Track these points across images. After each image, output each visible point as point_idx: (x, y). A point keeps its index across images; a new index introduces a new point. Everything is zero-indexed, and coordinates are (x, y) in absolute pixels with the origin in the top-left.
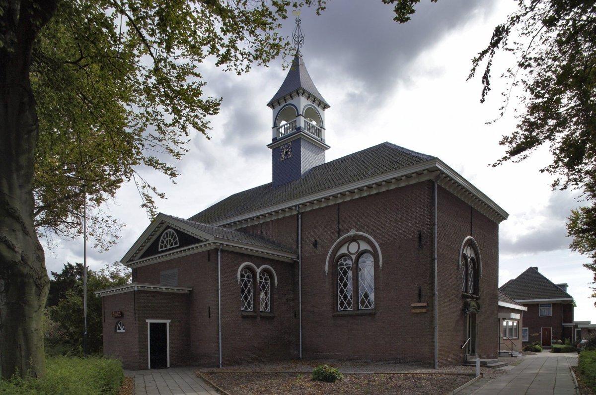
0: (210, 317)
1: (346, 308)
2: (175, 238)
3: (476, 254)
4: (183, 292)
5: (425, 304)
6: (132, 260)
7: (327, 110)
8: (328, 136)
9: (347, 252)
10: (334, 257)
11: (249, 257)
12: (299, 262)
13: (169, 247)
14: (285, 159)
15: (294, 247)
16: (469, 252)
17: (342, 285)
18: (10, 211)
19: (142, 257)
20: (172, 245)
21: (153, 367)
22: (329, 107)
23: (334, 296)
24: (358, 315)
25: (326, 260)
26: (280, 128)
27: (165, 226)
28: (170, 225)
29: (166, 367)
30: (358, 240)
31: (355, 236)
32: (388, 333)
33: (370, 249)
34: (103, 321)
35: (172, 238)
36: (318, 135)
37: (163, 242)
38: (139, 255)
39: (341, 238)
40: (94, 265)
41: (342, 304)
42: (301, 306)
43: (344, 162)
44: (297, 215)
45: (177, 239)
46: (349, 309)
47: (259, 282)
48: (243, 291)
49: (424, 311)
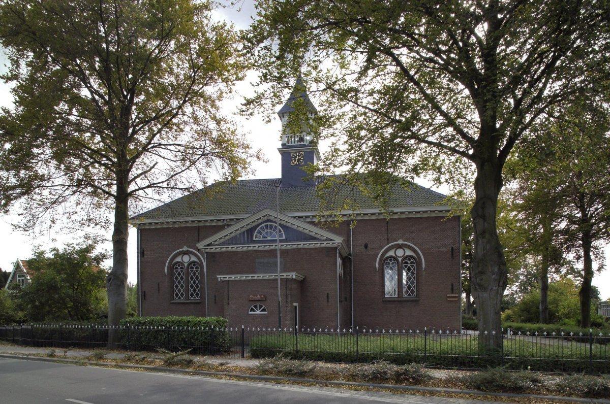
9: (394, 255)
14: (296, 165)
30: (405, 249)
31: (187, 251)
33: (198, 261)
40: (473, 177)
49: (456, 299)
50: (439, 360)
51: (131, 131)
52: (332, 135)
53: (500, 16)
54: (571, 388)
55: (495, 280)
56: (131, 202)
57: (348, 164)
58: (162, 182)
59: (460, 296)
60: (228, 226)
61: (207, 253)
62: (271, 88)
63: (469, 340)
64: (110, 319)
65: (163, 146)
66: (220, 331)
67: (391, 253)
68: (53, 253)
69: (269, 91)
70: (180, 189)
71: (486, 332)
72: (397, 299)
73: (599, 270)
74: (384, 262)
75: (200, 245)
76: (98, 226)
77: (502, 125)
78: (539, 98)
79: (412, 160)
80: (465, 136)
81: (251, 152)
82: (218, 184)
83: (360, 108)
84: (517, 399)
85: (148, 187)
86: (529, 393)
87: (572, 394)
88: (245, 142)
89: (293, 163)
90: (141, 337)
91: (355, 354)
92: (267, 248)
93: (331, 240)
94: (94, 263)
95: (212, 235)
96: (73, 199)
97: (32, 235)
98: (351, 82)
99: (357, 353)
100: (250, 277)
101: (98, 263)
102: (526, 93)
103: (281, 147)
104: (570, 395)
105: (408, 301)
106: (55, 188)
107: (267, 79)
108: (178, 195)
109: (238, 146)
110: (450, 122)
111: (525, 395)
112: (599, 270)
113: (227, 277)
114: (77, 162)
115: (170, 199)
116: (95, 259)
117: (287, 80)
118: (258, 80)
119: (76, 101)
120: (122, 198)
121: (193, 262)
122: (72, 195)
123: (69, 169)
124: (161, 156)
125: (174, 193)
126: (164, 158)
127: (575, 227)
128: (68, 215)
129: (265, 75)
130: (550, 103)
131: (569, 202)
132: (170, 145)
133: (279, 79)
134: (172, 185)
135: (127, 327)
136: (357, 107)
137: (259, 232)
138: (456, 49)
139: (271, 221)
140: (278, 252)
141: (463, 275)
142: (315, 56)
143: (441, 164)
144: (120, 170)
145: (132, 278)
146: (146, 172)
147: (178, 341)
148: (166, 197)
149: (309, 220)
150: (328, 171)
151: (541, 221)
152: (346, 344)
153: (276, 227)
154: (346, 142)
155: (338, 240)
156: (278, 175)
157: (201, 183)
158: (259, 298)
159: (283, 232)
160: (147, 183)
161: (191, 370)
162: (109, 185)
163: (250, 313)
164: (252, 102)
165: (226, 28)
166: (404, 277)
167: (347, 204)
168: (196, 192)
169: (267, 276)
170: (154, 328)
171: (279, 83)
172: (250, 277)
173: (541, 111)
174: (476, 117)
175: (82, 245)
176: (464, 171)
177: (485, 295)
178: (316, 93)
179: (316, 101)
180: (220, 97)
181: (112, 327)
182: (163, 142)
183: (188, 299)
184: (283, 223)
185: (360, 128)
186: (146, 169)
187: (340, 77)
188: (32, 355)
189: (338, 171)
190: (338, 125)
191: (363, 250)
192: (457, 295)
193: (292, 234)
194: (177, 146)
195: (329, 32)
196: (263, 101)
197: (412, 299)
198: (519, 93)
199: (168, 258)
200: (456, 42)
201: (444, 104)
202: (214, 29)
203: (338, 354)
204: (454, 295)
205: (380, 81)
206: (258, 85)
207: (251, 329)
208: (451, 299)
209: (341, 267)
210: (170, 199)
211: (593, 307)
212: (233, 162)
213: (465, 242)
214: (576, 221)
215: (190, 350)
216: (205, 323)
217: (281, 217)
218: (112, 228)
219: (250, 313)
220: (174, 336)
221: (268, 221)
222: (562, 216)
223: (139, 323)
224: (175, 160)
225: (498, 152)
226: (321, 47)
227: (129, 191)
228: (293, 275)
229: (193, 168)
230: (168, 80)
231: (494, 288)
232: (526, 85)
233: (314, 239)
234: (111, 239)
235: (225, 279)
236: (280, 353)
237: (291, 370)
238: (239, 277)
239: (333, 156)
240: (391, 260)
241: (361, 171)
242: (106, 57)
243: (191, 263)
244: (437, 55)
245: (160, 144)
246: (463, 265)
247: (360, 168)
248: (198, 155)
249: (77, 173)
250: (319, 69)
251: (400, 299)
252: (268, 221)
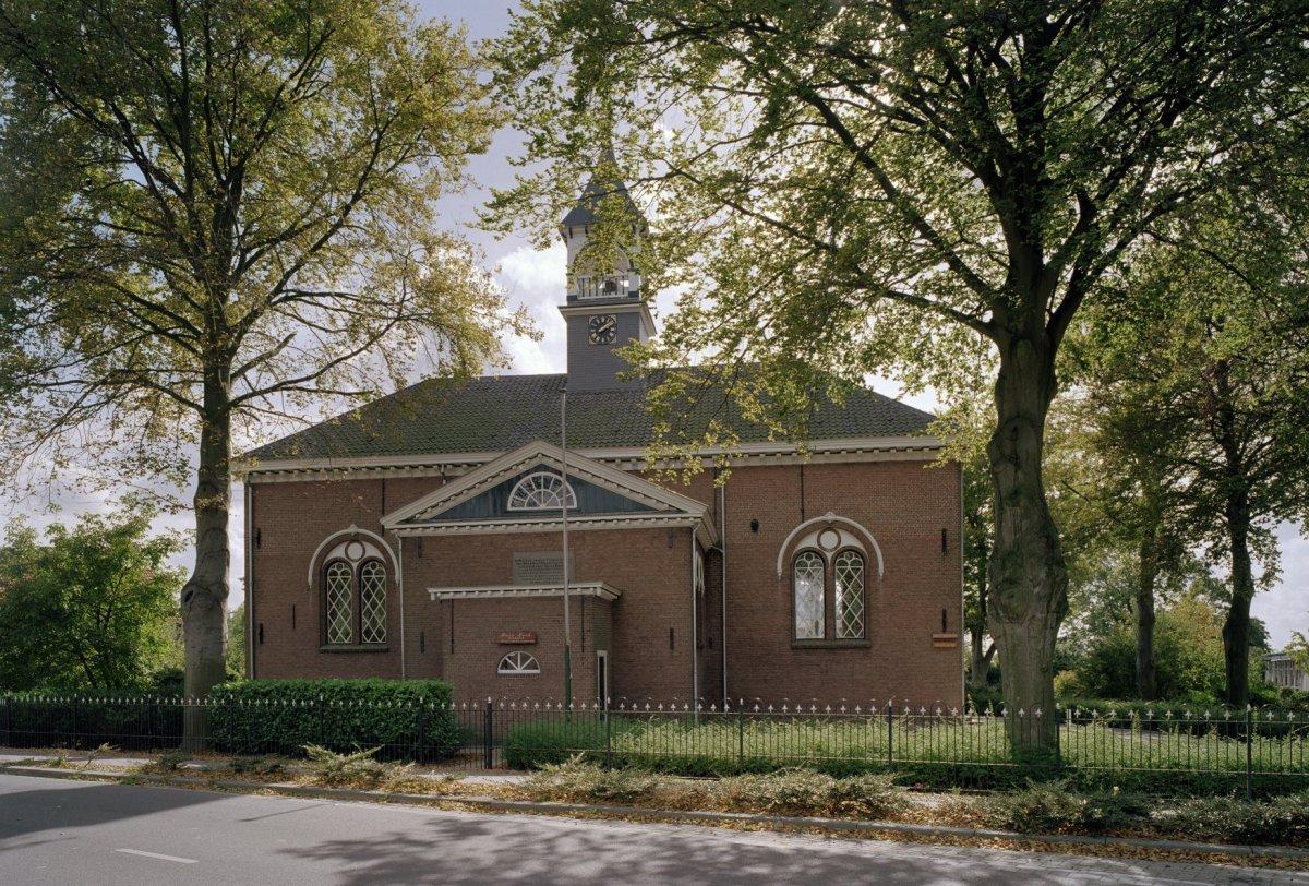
9: (343, 556)
18: (1121, 181)
25: (777, 554)
30: (840, 532)
31: (357, 534)
34: (446, 649)
39: (806, 523)
40: (991, 375)
49: (953, 645)
50: (921, 772)
51: (235, 261)
52: (683, 278)
53: (1050, 19)
54: (1208, 824)
55: (1040, 599)
56: (235, 421)
57: (720, 339)
58: (308, 378)
59: (960, 638)
60: (450, 479)
61: (403, 538)
62: (552, 171)
63: (985, 736)
64: (188, 685)
65: (307, 298)
66: (438, 711)
67: (810, 542)
68: (54, 535)
69: (547, 178)
70: (344, 394)
71: (1022, 712)
72: (823, 643)
73: (1267, 578)
74: (795, 561)
75: (389, 522)
76: (163, 477)
77: (1054, 257)
78: (1135, 198)
79: (864, 332)
80: (973, 281)
81: (504, 312)
82: (427, 385)
83: (747, 217)
84: (1092, 847)
85: (274, 389)
86: (1118, 836)
87: (1210, 837)
88: (489, 291)
89: (594, 340)
90: (260, 725)
91: (737, 759)
92: (538, 528)
93: (680, 511)
94: (148, 561)
95: (412, 500)
96: (107, 412)
97: (11, 492)
98: (727, 160)
99: (741, 757)
100: (500, 592)
101: (156, 560)
102: (1110, 185)
103: (565, 304)
104: (1206, 839)
105: (846, 648)
106: (63, 388)
107: (545, 151)
108: (339, 407)
109: (473, 300)
110: (941, 249)
111: (1109, 840)
112: (1267, 578)
113: (450, 593)
114: (109, 332)
115: (324, 416)
116: (148, 551)
117: (589, 153)
118: (525, 152)
119: (106, 195)
120: (217, 414)
121: (372, 559)
122: (106, 403)
123: (91, 348)
124: (303, 321)
125: (332, 405)
126: (310, 324)
127: (1209, 488)
128: (94, 450)
129: (540, 141)
130: (1157, 211)
131: (1199, 431)
132: (323, 295)
133: (570, 151)
134: (328, 386)
135: (228, 701)
136: (741, 217)
137: (520, 493)
138: (957, 89)
139: (546, 468)
140: (565, 536)
141: (966, 593)
142: (650, 101)
143: (922, 344)
144: (214, 351)
145: (236, 600)
146: (270, 355)
147: (344, 733)
148: (316, 412)
149: (629, 466)
150: (675, 359)
151: (1137, 473)
152: (714, 741)
153: (557, 483)
154: (713, 295)
155: (695, 510)
156: (563, 370)
157: (392, 382)
158: (520, 638)
159: (573, 493)
160: (273, 382)
161: (380, 791)
162: (187, 383)
163: (501, 672)
164: (509, 200)
165: (449, 34)
166: (837, 594)
167: (713, 432)
168: (383, 400)
169: (540, 591)
170: (290, 705)
171: (570, 160)
172: (500, 592)
173: (1135, 230)
174: (997, 237)
175: (120, 518)
176: (972, 362)
177: (1019, 630)
178: (652, 182)
179: (650, 202)
180: (432, 192)
181: (194, 702)
182: (303, 287)
183: (360, 643)
184: (574, 473)
185: (748, 262)
186: (271, 348)
187: (702, 148)
188: (15, 764)
189: (696, 358)
190: (698, 257)
191: (749, 534)
192: (955, 636)
193: (595, 498)
194: (342, 300)
195: (679, 47)
196: (535, 200)
198: (1093, 188)
199: (313, 550)
200: (955, 74)
201: (928, 211)
202: (422, 35)
203: (700, 759)
204: (950, 636)
205: (791, 159)
206: (523, 164)
207: (507, 706)
208: (943, 645)
209: (702, 572)
210: (324, 416)
211: (1253, 663)
212: (459, 335)
213: (971, 522)
214: (1214, 472)
215: (376, 749)
216: (404, 693)
217: (570, 458)
218: (194, 481)
219: (501, 672)
220: (334, 722)
221: (541, 468)
222: (1185, 461)
223: (256, 692)
224: (332, 329)
225: (1048, 318)
226: (663, 81)
227: (232, 396)
228: (596, 588)
229: (375, 347)
230: (316, 148)
231: (1039, 615)
232: (1107, 170)
233: (641, 508)
234: (191, 504)
235: (446, 597)
236: (576, 755)
237: (604, 790)
238: (476, 593)
239: (687, 325)
240: (809, 558)
241: (748, 358)
242: (179, 96)
243: (367, 562)
244: (914, 103)
245: (301, 294)
246: (967, 569)
247: (746, 352)
248: (388, 318)
249: (110, 357)
250: (655, 130)
251: (828, 644)
252: (541, 468)
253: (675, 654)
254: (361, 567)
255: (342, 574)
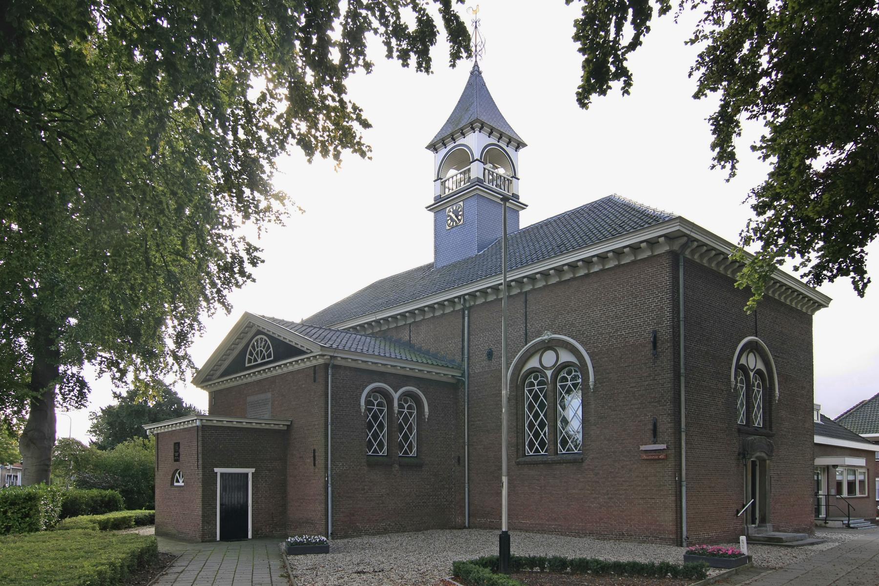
0: (315, 465)
1: (537, 451)
2: (268, 348)
3: (767, 363)
4: (276, 427)
5: (663, 446)
6: (210, 380)
7: (522, 151)
8: (524, 190)
9: (539, 366)
10: (520, 373)
11: (382, 376)
12: (464, 382)
13: (259, 361)
15: (458, 358)
16: (752, 362)
17: (531, 417)
19: (222, 376)
20: (264, 358)
21: (225, 537)
22: (525, 145)
23: (517, 432)
24: (554, 463)
26: (446, 181)
27: (254, 331)
28: (261, 329)
29: (214, 540)
30: (557, 349)
31: (551, 340)
32: (604, 491)
34: (156, 469)
35: (264, 348)
36: (506, 189)
37: (251, 354)
38: (219, 373)
41: (531, 445)
42: (468, 448)
43: (544, 227)
44: (463, 310)
45: (271, 349)
46: (542, 453)
47: (396, 412)
48: (370, 426)
197: (540, 458)
253: (316, 470)
254: (555, 376)
255: (573, 379)
